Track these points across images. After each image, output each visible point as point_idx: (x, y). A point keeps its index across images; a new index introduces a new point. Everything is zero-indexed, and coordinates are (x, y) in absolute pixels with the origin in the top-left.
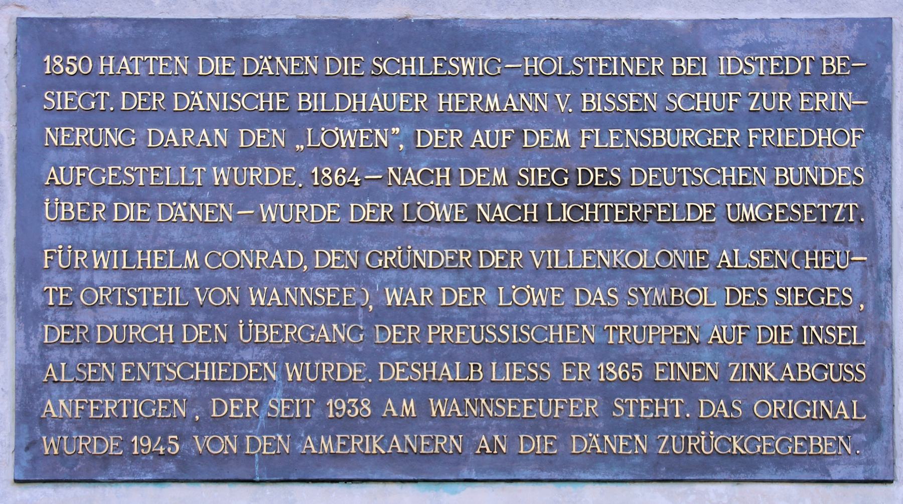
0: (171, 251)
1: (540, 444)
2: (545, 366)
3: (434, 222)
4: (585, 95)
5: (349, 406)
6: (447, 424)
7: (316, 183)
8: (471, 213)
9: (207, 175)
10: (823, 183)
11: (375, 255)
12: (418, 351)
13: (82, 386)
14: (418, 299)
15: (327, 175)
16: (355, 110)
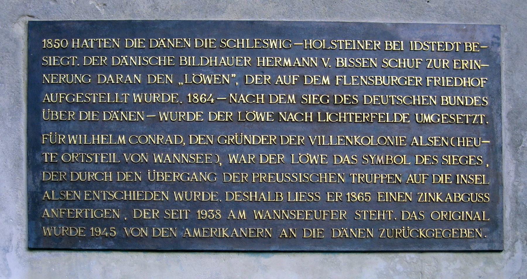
0: (111, 135)
2: (317, 194)
4: (338, 59)
5: (209, 213)
6: (265, 223)
7: (190, 101)
8: (276, 117)
9: (131, 98)
10: (467, 104)
11: (223, 138)
13: (63, 202)
14: (247, 160)
15: (196, 98)
16: (211, 65)
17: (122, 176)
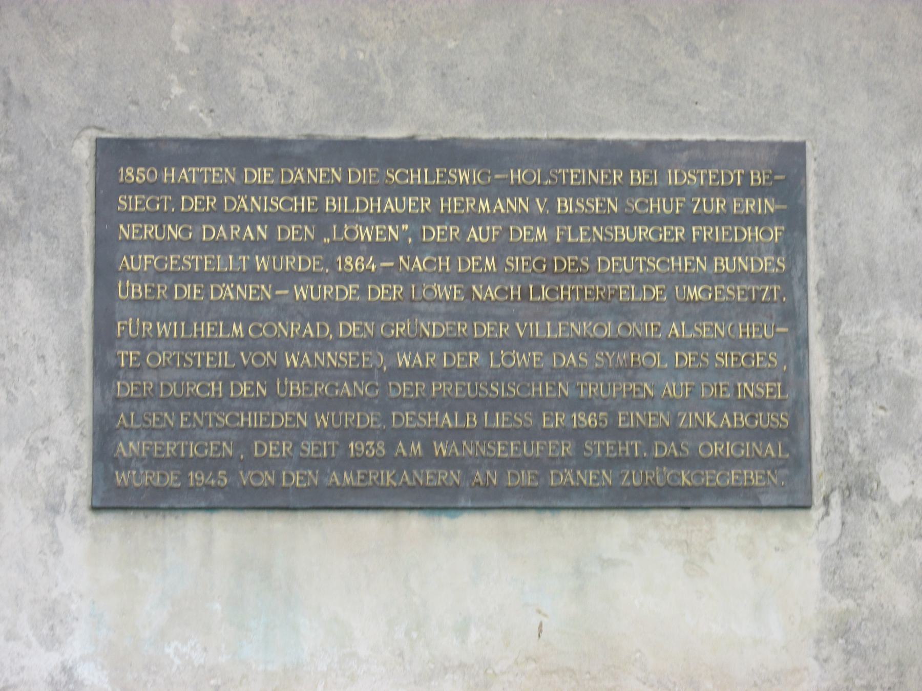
1: (526, 478)
3: (437, 300)
6: (449, 462)
9: (251, 264)
12: (423, 403)
14: (424, 361)
17: (237, 389)
